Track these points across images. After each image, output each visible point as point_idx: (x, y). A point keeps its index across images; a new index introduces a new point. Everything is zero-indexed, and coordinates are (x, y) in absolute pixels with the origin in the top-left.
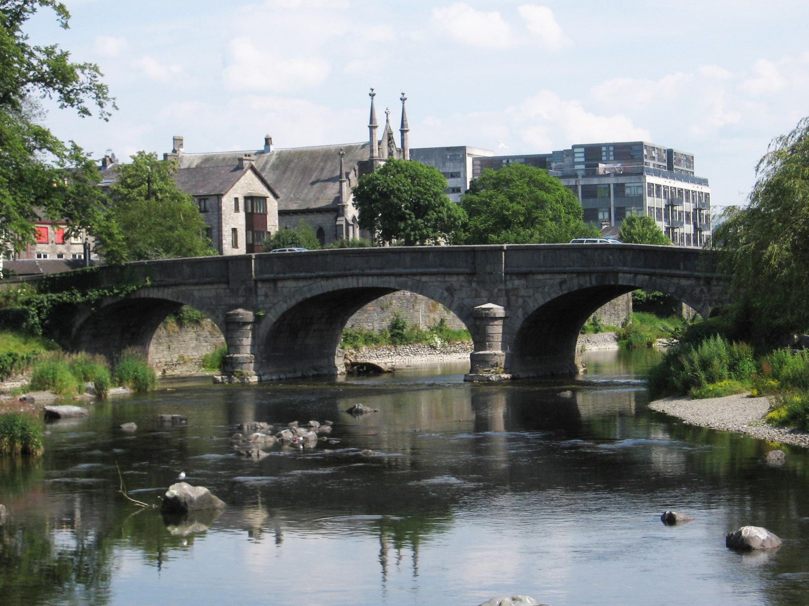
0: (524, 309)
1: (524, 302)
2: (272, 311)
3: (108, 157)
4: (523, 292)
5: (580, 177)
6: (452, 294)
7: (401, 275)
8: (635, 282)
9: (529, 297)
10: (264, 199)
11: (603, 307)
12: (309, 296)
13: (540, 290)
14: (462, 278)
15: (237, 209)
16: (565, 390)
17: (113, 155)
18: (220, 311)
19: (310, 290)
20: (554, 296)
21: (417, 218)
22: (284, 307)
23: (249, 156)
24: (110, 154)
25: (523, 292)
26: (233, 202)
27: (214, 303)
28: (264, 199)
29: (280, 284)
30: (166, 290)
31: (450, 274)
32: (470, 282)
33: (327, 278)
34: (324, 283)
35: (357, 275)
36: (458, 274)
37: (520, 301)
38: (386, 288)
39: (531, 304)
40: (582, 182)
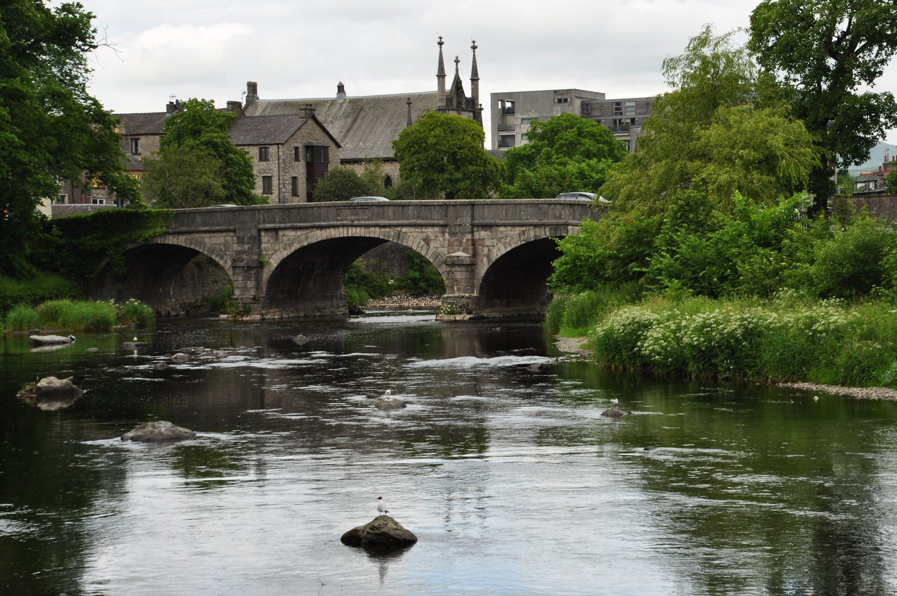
0: (488, 256)
1: (489, 250)
4: (488, 242)
7: (384, 226)
10: (326, 148)
11: (509, 249)
12: (306, 244)
14: (437, 229)
15: (297, 159)
20: (514, 246)
22: (285, 254)
25: (488, 242)
28: (326, 148)
29: (281, 233)
30: (180, 237)
31: (427, 226)
32: (443, 233)
33: (321, 228)
34: (318, 232)
35: (348, 226)
36: (433, 226)
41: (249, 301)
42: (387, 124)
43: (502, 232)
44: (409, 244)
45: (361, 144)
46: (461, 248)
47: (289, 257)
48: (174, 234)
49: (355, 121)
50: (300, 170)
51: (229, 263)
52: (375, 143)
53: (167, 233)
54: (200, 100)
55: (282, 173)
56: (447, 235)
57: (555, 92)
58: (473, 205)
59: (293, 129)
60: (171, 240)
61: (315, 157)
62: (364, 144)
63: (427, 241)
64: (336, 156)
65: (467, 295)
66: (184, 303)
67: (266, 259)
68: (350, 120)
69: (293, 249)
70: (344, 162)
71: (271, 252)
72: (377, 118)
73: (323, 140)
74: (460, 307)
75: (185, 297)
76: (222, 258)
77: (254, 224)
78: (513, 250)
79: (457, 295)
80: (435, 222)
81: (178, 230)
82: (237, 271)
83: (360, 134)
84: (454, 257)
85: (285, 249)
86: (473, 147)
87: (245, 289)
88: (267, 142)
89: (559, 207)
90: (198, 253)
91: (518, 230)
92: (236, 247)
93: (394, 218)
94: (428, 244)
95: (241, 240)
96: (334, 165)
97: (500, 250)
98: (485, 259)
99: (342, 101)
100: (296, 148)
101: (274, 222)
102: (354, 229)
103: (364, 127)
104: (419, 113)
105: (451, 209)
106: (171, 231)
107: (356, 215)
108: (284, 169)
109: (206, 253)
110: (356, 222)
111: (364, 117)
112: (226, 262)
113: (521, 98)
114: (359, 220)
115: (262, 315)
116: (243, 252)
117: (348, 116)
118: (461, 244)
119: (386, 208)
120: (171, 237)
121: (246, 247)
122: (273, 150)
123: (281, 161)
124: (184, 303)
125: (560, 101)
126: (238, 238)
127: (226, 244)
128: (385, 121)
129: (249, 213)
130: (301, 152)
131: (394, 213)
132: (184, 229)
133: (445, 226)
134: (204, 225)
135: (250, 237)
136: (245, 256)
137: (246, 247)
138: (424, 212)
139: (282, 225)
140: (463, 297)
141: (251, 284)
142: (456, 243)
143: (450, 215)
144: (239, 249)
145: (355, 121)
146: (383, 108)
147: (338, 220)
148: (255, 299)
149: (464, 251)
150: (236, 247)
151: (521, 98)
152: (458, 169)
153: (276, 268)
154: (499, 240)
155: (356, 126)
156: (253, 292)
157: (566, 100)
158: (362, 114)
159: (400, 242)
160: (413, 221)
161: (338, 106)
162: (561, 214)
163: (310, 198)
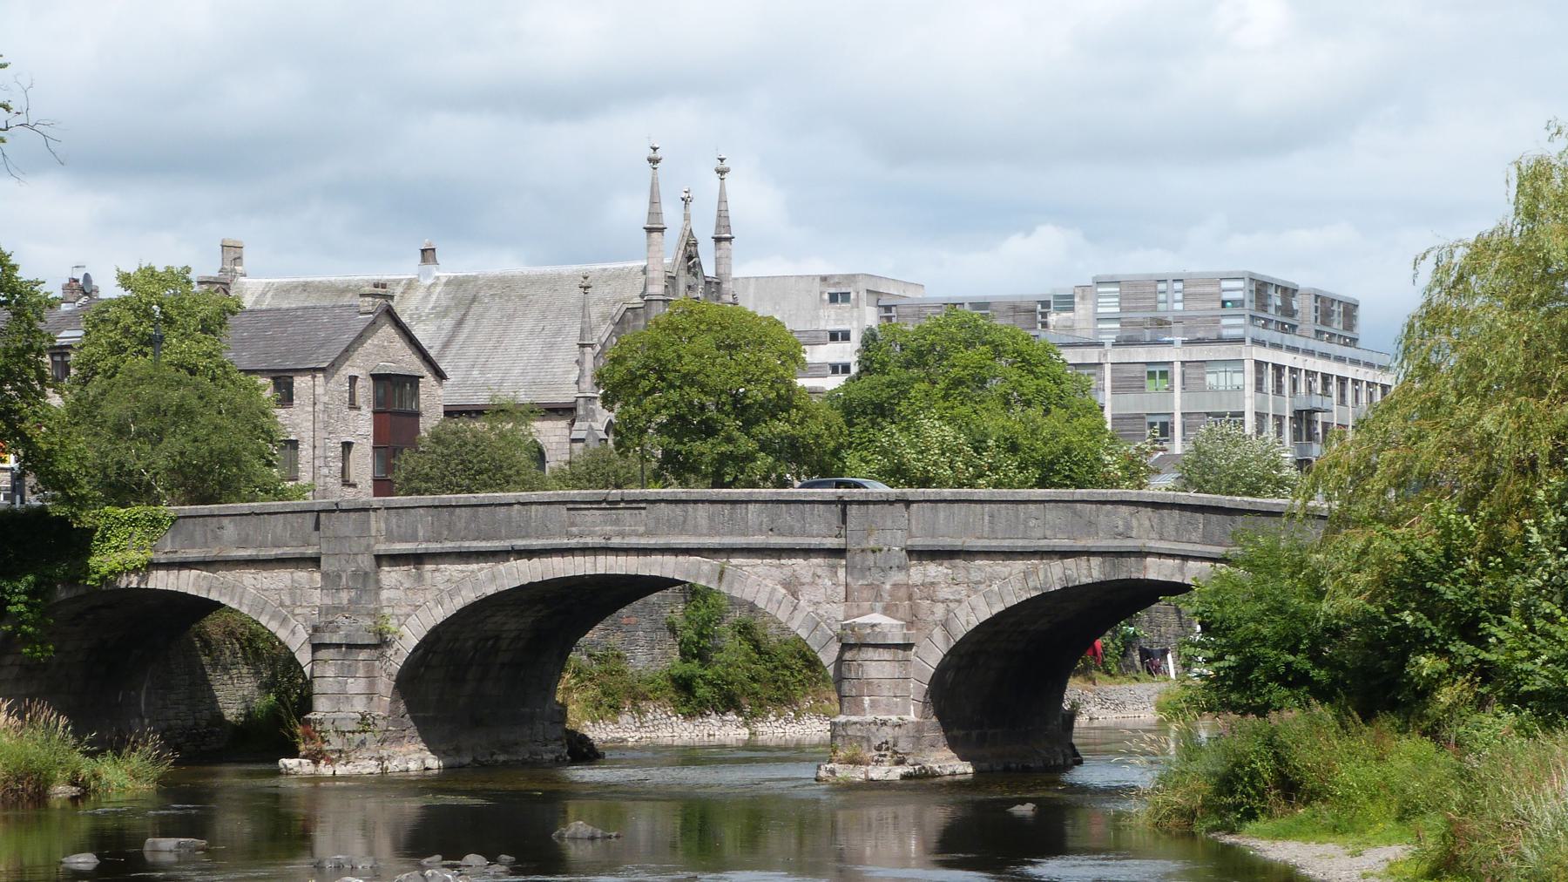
0: (945, 625)
1: (948, 611)
2: (413, 620)
3: (76, 281)
4: (944, 592)
5: (1108, 346)
6: (794, 594)
8: (1183, 574)
9: (959, 601)
10: (414, 380)
11: (999, 608)
12: (490, 591)
13: (982, 587)
15: (353, 405)
16: (1023, 802)
17: (87, 276)
18: (300, 619)
19: (494, 578)
20: (1012, 601)
21: (661, 429)
22: (440, 614)
23: (384, 286)
24: (79, 276)
25: (944, 592)
26: (442, 366)
27: (288, 603)
28: (414, 380)
30: (185, 573)
32: (833, 569)
33: (529, 553)
34: (523, 564)
37: (940, 610)
38: (667, 579)
39: (963, 619)
40: (1114, 355)
41: (354, 727)
42: (532, 332)
43: (980, 569)
44: (748, 595)
45: (475, 373)
46: (879, 605)
47: (447, 623)
48: (169, 566)
49: (460, 323)
50: (362, 426)
51: (303, 635)
52: (507, 371)
53: (153, 565)
54: (160, 269)
55: (321, 434)
56: (841, 573)
57: (824, 279)
58: (844, 504)
59: (348, 338)
60: (161, 581)
61: (394, 395)
62: (482, 373)
63: (793, 587)
64: (433, 400)
65: (894, 718)
66: (170, 728)
67: (392, 625)
68: (448, 323)
69: (459, 603)
70: (451, 413)
71: (407, 610)
72: (511, 317)
73: (409, 363)
74: (879, 748)
75: (171, 713)
76: (284, 621)
77: (364, 542)
78: (1009, 611)
79: (869, 718)
80: (814, 542)
81: (178, 557)
82: (323, 654)
83: (472, 351)
84: (864, 625)
85: (440, 602)
86: (782, 379)
87: (342, 696)
88: (289, 365)
89: (1124, 509)
90: (218, 605)
91: (1019, 565)
92: (317, 598)
93: (713, 531)
94: (794, 594)
95: (332, 582)
96: (430, 420)
97: (974, 611)
98: (938, 634)
99: (429, 282)
100: (353, 379)
101: (414, 538)
102: (611, 559)
103: (480, 337)
104: (602, 308)
105: (853, 510)
106: (163, 558)
107: (617, 522)
108: (326, 425)
109: (245, 610)
110: (616, 541)
111: (482, 316)
112: (293, 632)
113: (751, 290)
114: (622, 534)
115: (381, 759)
116: (337, 609)
117: (444, 313)
118: (878, 596)
119: (690, 507)
120: (161, 573)
121: (344, 597)
122: (301, 383)
123: (319, 407)
124: (170, 728)
125: (833, 298)
126: (325, 576)
127: (293, 590)
128: (529, 324)
129: (353, 516)
130: (365, 390)
131: (711, 518)
132: (194, 554)
133: (839, 553)
134: (243, 543)
135: (355, 573)
136: (341, 619)
137: (344, 597)
138: (787, 516)
139: (434, 547)
140: (884, 723)
141: (356, 685)
142: (866, 594)
143: (852, 522)
144: (328, 601)
145: (460, 323)
146: (522, 297)
147: (570, 535)
148: (365, 721)
149: (887, 611)
150: (317, 598)
151: (751, 290)
152: (746, 428)
153: (416, 649)
154: (974, 586)
155: (461, 337)
156: (360, 706)
157: (846, 297)
158: (476, 309)
159: (723, 589)
160: (758, 540)
161: (421, 293)
162: (1128, 527)
163: (382, 486)
